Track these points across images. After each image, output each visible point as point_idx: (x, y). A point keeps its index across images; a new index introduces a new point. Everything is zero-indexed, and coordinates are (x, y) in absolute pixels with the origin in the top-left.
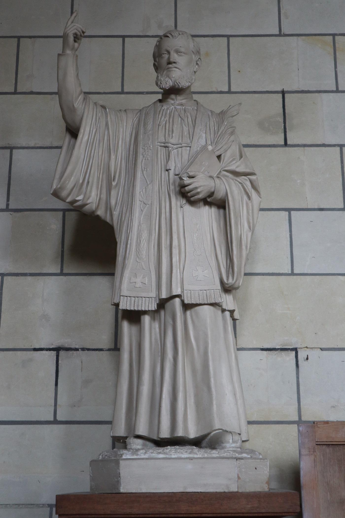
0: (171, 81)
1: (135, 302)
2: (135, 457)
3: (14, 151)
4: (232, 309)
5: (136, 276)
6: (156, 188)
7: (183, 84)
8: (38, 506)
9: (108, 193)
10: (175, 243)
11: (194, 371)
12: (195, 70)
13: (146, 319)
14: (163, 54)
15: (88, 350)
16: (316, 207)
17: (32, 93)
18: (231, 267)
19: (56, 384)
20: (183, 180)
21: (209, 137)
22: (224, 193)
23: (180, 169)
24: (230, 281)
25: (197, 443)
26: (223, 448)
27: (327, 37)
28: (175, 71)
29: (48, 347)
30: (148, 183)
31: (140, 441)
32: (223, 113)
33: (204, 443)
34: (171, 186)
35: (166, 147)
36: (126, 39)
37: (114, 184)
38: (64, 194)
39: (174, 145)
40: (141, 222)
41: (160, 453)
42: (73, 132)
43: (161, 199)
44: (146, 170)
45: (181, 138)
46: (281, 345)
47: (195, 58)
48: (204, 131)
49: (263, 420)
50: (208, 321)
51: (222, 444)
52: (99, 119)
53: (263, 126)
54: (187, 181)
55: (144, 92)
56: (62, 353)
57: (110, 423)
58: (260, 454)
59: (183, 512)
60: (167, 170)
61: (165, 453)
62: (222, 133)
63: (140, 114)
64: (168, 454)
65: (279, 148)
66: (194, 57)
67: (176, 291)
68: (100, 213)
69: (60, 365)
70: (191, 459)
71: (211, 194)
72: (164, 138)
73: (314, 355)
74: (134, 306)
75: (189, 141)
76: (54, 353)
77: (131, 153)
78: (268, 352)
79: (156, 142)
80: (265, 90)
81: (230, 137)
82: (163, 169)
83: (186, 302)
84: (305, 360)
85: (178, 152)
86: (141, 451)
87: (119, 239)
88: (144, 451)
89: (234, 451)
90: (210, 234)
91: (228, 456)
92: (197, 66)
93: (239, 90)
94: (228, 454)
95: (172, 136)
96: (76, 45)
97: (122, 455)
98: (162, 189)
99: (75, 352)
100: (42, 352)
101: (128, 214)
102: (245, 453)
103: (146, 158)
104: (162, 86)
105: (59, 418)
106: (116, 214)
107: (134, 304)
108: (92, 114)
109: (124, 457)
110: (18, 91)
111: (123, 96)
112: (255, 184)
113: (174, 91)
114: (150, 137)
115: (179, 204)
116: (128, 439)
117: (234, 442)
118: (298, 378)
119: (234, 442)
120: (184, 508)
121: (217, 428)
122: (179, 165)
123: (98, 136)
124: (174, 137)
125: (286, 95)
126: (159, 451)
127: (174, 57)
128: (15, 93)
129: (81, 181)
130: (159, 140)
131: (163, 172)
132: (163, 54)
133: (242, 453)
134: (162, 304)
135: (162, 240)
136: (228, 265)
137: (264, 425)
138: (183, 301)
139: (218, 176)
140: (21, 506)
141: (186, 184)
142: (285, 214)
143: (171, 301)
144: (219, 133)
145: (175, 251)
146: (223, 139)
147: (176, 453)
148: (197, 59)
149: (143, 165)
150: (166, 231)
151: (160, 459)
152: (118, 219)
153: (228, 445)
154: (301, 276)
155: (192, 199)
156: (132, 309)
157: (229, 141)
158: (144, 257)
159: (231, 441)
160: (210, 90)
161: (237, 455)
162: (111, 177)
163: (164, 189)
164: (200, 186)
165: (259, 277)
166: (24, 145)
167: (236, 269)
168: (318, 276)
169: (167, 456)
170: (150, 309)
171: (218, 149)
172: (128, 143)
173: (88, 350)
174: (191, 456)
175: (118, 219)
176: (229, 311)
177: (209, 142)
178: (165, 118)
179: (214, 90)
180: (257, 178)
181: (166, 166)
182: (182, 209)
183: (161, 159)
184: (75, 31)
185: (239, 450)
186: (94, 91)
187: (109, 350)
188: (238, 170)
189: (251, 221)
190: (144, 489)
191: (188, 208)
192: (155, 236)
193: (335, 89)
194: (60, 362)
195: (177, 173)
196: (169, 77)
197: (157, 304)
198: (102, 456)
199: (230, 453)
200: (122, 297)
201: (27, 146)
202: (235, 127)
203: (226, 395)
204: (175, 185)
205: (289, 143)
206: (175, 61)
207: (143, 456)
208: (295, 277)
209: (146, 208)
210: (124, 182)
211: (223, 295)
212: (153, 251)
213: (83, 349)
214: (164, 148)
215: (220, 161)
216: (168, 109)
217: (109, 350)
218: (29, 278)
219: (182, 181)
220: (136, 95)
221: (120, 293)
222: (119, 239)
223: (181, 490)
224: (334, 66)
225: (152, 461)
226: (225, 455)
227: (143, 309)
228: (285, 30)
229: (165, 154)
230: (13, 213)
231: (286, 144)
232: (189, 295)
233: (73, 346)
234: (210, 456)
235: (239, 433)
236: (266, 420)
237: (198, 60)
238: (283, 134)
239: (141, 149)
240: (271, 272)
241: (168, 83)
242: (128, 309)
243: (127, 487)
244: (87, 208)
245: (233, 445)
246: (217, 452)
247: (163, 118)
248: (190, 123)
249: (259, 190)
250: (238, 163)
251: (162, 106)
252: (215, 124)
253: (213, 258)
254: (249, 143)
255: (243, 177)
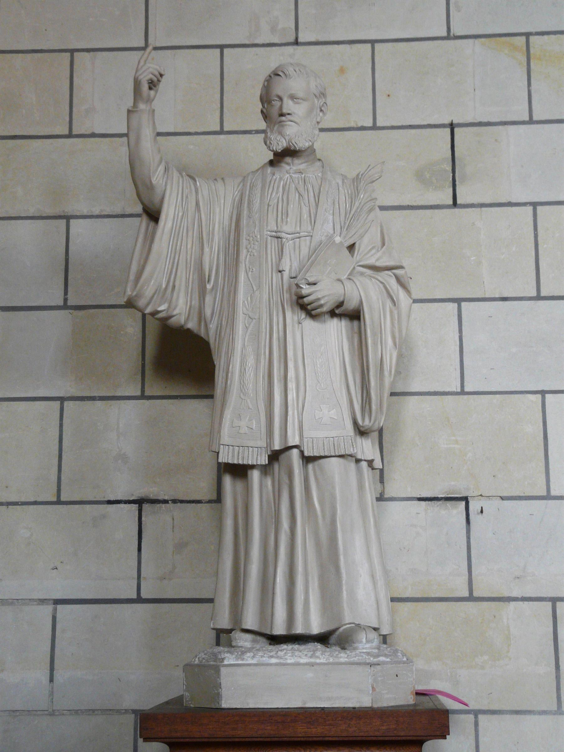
0: (284, 141)
1: (239, 453)
2: (240, 662)
3: (72, 222)
4: (370, 458)
5: (239, 417)
6: (266, 296)
7: (301, 144)
8: (118, 712)
9: (202, 298)
10: (291, 374)
11: (318, 544)
12: (318, 120)
13: (255, 475)
14: (273, 100)
15: (182, 502)
16: (497, 296)
17: (93, 135)
18: (367, 403)
19: (139, 549)
20: (302, 288)
21: (338, 220)
22: (358, 300)
23: (298, 270)
24: (367, 422)
25: (323, 639)
26: (355, 649)
27: (518, 38)
28: (289, 125)
29: (127, 499)
30: (255, 289)
31: (248, 636)
32: (357, 179)
33: (333, 639)
34: (285, 295)
35: (278, 237)
36: (226, 51)
37: (209, 287)
38: (141, 303)
39: (289, 234)
40: (246, 344)
41: (272, 657)
42: (153, 215)
43: (271, 310)
44: (251, 270)
45: (298, 224)
46: (446, 492)
47: (318, 103)
48: (331, 212)
49: (420, 596)
50: (337, 479)
51: (353, 645)
52: (187, 197)
53: (422, 177)
54: (306, 289)
55: (252, 131)
56: (145, 506)
57: (211, 601)
58: (404, 655)
59: (300, 735)
60: (280, 272)
61: (277, 657)
62: (356, 211)
63: (243, 185)
64: (281, 658)
65: (444, 211)
66: (316, 102)
67: (293, 440)
68: (191, 325)
69: (143, 523)
70: (312, 665)
71: (340, 305)
72: (275, 225)
73: (490, 506)
74: (238, 459)
75: (310, 229)
76: (135, 507)
77: (232, 243)
78: (427, 502)
79: (265, 230)
80: (425, 123)
81: (367, 216)
82: (274, 269)
83: (306, 454)
84: (478, 514)
85: (294, 243)
86: (248, 654)
87: (218, 363)
88: (252, 654)
89: (368, 654)
90: (340, 360)
91: (360, 661)
92: (321, 114)
93: (388, 124)
94: (360, 658)
95: (287, 222)
96: (152, 93)
97: (223, 660)
98: (273, 298)
99: (163, 505)
100: (119, 505)
101: (228, 331)
102: (382, 656)
103: (252, 254)
104: (273, 148)
105: (144, 595)
106: (212, 327)
107: (238, 456)
108: (176, 191)
109: (226, 662)
110: (75, 132)
111: (222, 137)
112: (402, 280)
113: (287, 154)
114: (257, 223)
115: (296, 318)
116: (233, 632)
117: (368, 641)
118: (468, 538)
119: (368, 641)
120: (301, 731)
121: (347, 622)
122: (295, 264)
123: (186, 223)
124: (289, 223)
125: (456, 130)
126: (271, 654)
127: (289, 106)
128: (70, 135)
129: (164, 286)
130: (269, 228)
131: (274, 275)
132: (273, 100)
133: (378, 656)
134: (274, 456)
135: (273, 371)
136: (365, 399)
137: (422, 603)
138: (302, 452)
139: (350, 277)
140: (96, 712)
141: (305, 295)
142: (453, 306)
143: (287, 453)
144: (352, 213)
145: (291, 385)
146: (358, 220)
147: (292, 656)
148: (322, 104)
149: (247, 263)
150: (280, 356)
151: (271, 665)
152: (216, 334)
153: (360, 646)
154: (475, 396)
155: (313, 313)
156: (236, 462)
157: (367, 221)
158: (251, 391)
159: (364, 640)
160: (347, 125)
161: (372, 659)
162: (205, 278)
163: (276, 298)
164: (323, 297)
165: (416, 397)
166: (85, 212)
167: (374, 407)
168: (498, 396)
169: (282, 661)
170: (259, 463)
171: (351, 235)
172: (227, 229)
173: (182, 502)
174: (312, 660)
175: (216, 334)
176: (365, 460)
177: (338, 227)
178: (277, 193)
179: (352, 124)
180: (406, 272)
181: (278, 265)
182: (300, 325)
183: (271, 255)
184: (151, 76)
185: (376, 651)
186: (182, 131)
187: (210, 502)
188: (378, 264)
189: (397, 335)
190: (252, 703)
191: (309, 323)
192: (264, 363)
193: (527, 119)
194: (143, 519)
195: (293, 275)
196: (281, 135)
197: (269, 456)
198: (199, 658)
199: (363, 656)
200: (222, 446)
201: (90, 214)
202: (376, 199)
203: (361, 576)
204: (291, 294)
205: (459, 201)
206: (289, 112)
207: (250, 661)
208: (466, 397)
209: (252, 324)
210: (222, 283)
211: (359, 439)
212: (262, 384)
213: (175, 501)
214: (276, 239)
215: (353, 256)
216: (281, 179)
217: (210, 502)
218: (99, 403)
219: (299, 290)
220: (241, 136)
221: (219, 441)
222: (218, 363)
223: (299, 704)
224: (526, 83)
225: (262, 667)
226: (356, 659)
227: (250, 463)
228: (457, 30)
229: (277, 248)
230: (73, 311)
231: (455, 204)
232: (310, 445)
233: (160, 498)
234: (337, 660)
235: (376, 626)
236: (425, 596)
237: (323, 105)
238: (451, 189)
239: (244, 240)
240: (432, 390)
241: (280, 144)
242: (230, 462)
243: (229, 701)
244: (173, 321)
245: (368, 646)
246: (346, 656)
247: (274, 194)
248: (312, 199)
249: (409, 289)
250: (379, 254)
251: (274, 174)
252: (347, 198)
253: (343, 388)
254: (402, 204)
255: (387, 272)
